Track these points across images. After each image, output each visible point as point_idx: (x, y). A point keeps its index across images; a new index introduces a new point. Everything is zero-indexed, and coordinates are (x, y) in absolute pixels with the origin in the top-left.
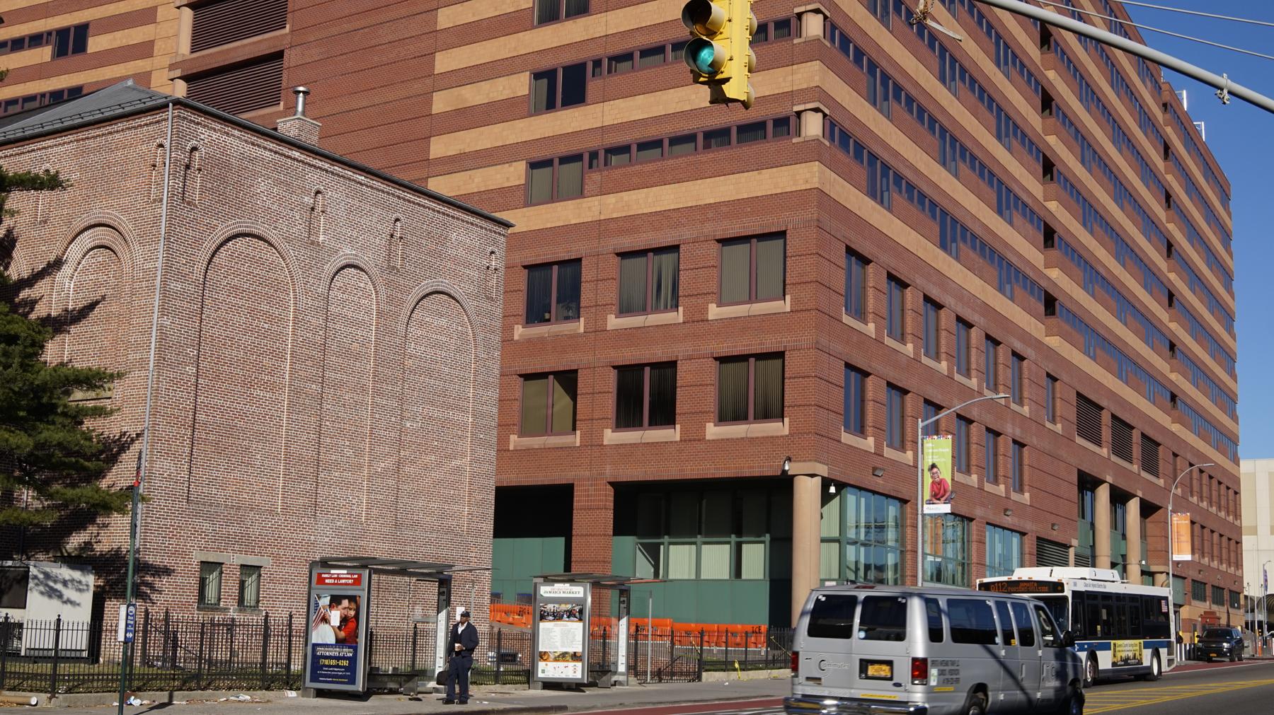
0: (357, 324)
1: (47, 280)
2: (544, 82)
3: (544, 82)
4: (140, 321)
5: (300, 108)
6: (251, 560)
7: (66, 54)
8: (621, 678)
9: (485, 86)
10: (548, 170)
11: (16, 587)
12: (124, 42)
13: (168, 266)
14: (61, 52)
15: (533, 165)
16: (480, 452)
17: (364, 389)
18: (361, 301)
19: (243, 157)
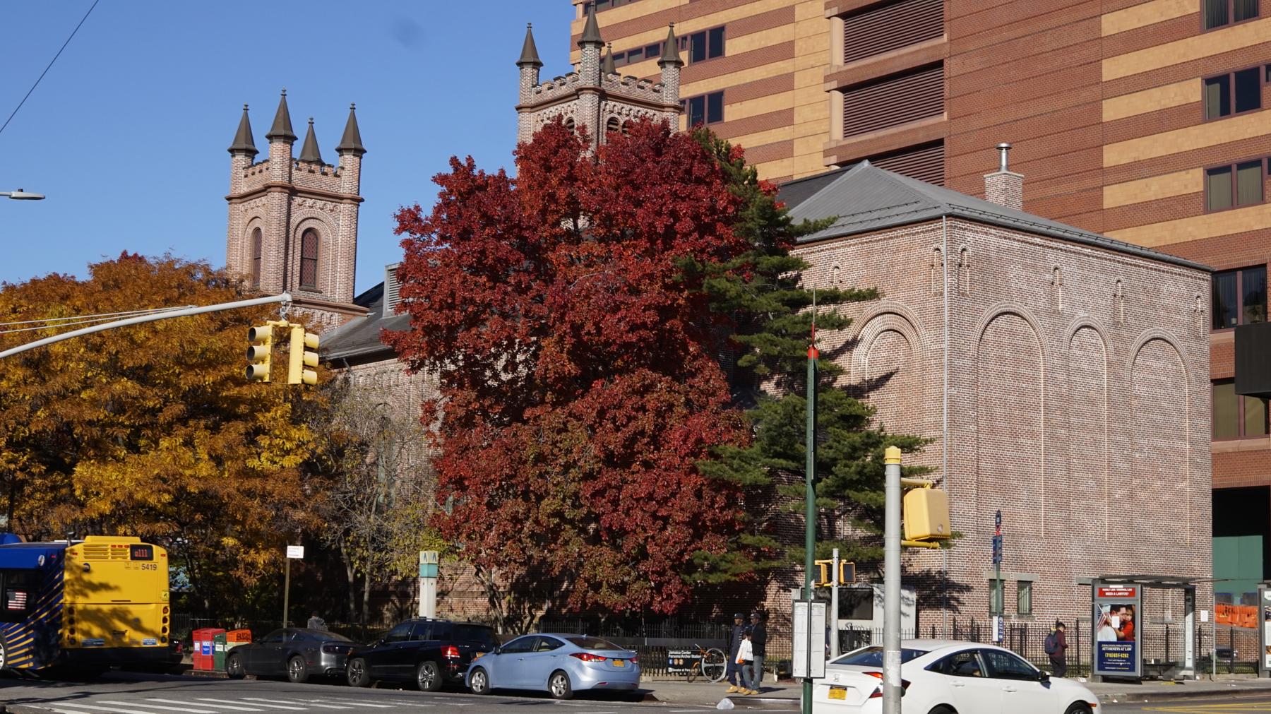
0: (1092, 375)
1: (847, 354)
2: (1216, 87)
3: (1216, 87)
4: (933, 391)
5: (1004, 163)
6: (1025, 577)
7: (703, 58)
8: (1190, 673)
9: (1156, 92)
10: (1226, 176)
11: (864, 603)
12: (763, 44)
13: (952, 346)
14: (697, 57)
15: (1211, 172)
16: (1198, 473)
17: (1101, 430)
18: (1094, 355)
19: (999, 250)
